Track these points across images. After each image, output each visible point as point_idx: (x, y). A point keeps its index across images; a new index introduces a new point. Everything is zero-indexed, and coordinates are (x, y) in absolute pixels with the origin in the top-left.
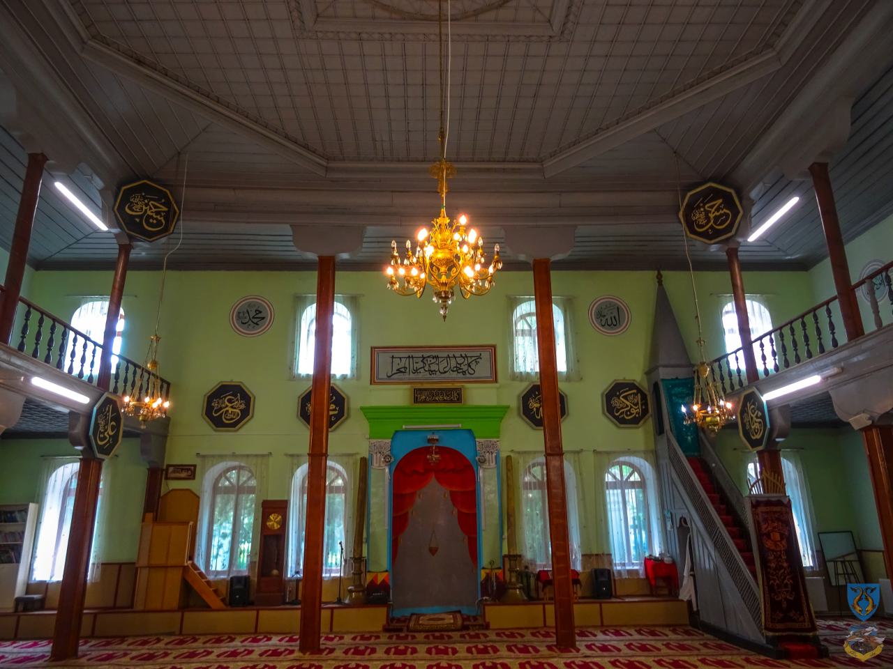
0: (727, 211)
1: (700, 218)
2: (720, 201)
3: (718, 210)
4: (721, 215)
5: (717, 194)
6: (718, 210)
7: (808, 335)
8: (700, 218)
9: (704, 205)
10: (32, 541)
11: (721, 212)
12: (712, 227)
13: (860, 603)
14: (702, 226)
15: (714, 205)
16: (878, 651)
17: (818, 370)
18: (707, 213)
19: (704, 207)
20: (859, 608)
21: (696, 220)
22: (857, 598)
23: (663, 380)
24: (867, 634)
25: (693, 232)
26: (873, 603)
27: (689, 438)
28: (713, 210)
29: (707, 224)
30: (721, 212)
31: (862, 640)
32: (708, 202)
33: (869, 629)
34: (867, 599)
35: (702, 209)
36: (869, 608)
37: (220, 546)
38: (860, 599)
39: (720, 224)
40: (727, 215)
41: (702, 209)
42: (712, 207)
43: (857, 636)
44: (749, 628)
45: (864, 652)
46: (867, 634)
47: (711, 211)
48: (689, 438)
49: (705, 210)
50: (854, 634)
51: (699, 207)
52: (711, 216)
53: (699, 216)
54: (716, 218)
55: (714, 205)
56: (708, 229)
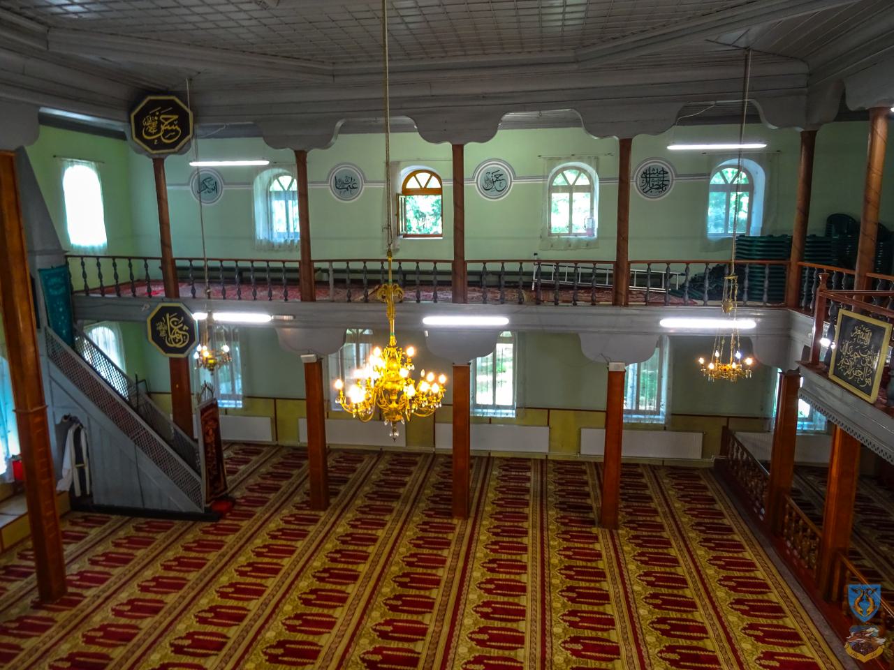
0: (179, 129)
1: (151, 125)
2: (176, 117)
3: (171, 124)
4: (172, 131)
5: (177, 109)
6: (171, 124)
7: (87, 272)
8: (151, 125)
9: (160, 114)
10: (449, 74)
11: (173, 127)
12: (159, 139)
13: (861, 603)
14: (150, 134)
15: (169, 119)
16: (879, 651)
17: (271, 312)
18: (160, 123)
19: (158, 116)
20: (860, 609)
21: (146, 127)
22: (858, 599)
23: (40, 270)
24: (868, 635)
25: (139, 135)
26: (874, 603)
27: (64, 332)
28: (166, 123)
29: (155, 134)
30: (173, 127)
31: (863, 641)
32: (165, 113)
33: (871, 629)
34: (868, 600)
35: (156, 118)
36: (870, 609)
37: (501, 414)
38: (862, 599)
39: (168, 139)
40: (177, 132)
41: (156, 118)
42: (166, 119)
43: (858, 637)
44: (181, 502)
45: (864, 654)
46: (868, 635)
47: (163, 124)
48: (64, 332)
49: (159, 120)
50: (855, 634)
51: (154, 115)
52: (163, 128)
53: (150, 124)
54: (166, 132)
55: (169, 119)
56: (154, 139)
